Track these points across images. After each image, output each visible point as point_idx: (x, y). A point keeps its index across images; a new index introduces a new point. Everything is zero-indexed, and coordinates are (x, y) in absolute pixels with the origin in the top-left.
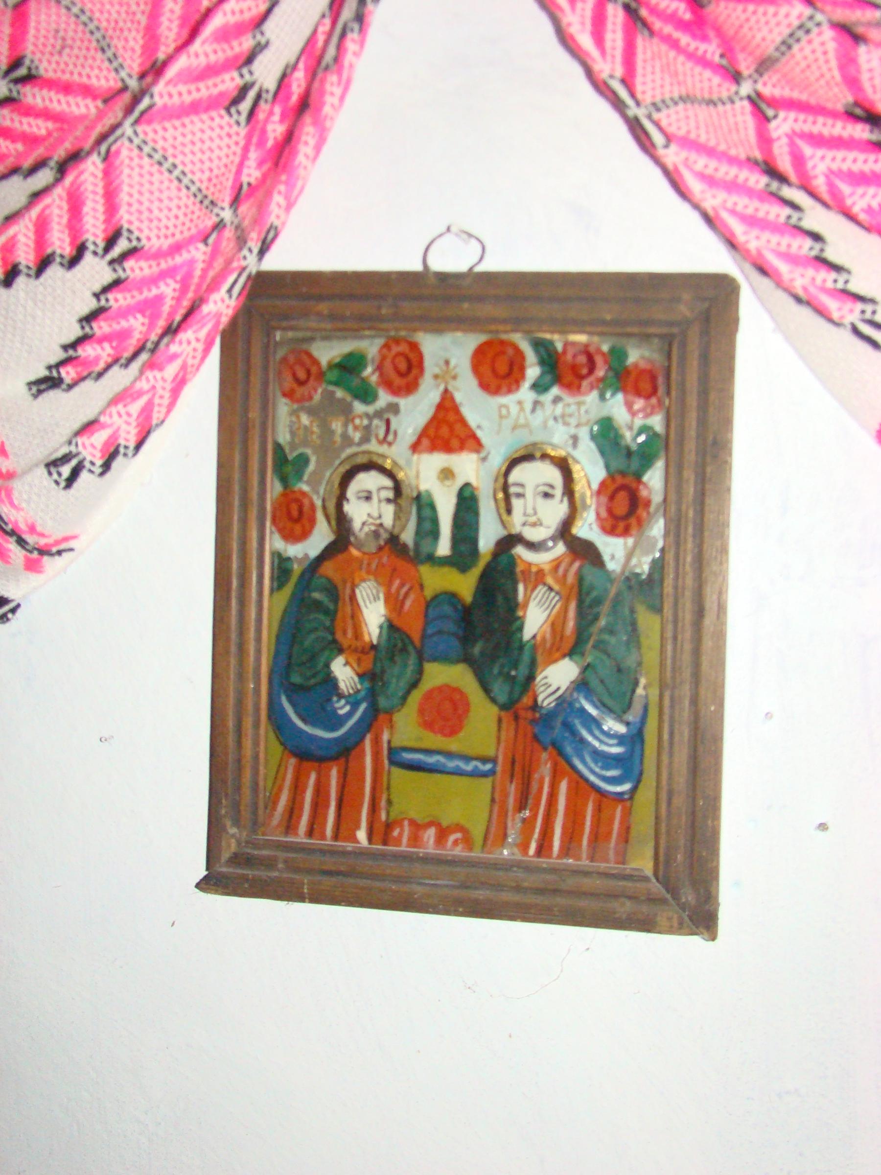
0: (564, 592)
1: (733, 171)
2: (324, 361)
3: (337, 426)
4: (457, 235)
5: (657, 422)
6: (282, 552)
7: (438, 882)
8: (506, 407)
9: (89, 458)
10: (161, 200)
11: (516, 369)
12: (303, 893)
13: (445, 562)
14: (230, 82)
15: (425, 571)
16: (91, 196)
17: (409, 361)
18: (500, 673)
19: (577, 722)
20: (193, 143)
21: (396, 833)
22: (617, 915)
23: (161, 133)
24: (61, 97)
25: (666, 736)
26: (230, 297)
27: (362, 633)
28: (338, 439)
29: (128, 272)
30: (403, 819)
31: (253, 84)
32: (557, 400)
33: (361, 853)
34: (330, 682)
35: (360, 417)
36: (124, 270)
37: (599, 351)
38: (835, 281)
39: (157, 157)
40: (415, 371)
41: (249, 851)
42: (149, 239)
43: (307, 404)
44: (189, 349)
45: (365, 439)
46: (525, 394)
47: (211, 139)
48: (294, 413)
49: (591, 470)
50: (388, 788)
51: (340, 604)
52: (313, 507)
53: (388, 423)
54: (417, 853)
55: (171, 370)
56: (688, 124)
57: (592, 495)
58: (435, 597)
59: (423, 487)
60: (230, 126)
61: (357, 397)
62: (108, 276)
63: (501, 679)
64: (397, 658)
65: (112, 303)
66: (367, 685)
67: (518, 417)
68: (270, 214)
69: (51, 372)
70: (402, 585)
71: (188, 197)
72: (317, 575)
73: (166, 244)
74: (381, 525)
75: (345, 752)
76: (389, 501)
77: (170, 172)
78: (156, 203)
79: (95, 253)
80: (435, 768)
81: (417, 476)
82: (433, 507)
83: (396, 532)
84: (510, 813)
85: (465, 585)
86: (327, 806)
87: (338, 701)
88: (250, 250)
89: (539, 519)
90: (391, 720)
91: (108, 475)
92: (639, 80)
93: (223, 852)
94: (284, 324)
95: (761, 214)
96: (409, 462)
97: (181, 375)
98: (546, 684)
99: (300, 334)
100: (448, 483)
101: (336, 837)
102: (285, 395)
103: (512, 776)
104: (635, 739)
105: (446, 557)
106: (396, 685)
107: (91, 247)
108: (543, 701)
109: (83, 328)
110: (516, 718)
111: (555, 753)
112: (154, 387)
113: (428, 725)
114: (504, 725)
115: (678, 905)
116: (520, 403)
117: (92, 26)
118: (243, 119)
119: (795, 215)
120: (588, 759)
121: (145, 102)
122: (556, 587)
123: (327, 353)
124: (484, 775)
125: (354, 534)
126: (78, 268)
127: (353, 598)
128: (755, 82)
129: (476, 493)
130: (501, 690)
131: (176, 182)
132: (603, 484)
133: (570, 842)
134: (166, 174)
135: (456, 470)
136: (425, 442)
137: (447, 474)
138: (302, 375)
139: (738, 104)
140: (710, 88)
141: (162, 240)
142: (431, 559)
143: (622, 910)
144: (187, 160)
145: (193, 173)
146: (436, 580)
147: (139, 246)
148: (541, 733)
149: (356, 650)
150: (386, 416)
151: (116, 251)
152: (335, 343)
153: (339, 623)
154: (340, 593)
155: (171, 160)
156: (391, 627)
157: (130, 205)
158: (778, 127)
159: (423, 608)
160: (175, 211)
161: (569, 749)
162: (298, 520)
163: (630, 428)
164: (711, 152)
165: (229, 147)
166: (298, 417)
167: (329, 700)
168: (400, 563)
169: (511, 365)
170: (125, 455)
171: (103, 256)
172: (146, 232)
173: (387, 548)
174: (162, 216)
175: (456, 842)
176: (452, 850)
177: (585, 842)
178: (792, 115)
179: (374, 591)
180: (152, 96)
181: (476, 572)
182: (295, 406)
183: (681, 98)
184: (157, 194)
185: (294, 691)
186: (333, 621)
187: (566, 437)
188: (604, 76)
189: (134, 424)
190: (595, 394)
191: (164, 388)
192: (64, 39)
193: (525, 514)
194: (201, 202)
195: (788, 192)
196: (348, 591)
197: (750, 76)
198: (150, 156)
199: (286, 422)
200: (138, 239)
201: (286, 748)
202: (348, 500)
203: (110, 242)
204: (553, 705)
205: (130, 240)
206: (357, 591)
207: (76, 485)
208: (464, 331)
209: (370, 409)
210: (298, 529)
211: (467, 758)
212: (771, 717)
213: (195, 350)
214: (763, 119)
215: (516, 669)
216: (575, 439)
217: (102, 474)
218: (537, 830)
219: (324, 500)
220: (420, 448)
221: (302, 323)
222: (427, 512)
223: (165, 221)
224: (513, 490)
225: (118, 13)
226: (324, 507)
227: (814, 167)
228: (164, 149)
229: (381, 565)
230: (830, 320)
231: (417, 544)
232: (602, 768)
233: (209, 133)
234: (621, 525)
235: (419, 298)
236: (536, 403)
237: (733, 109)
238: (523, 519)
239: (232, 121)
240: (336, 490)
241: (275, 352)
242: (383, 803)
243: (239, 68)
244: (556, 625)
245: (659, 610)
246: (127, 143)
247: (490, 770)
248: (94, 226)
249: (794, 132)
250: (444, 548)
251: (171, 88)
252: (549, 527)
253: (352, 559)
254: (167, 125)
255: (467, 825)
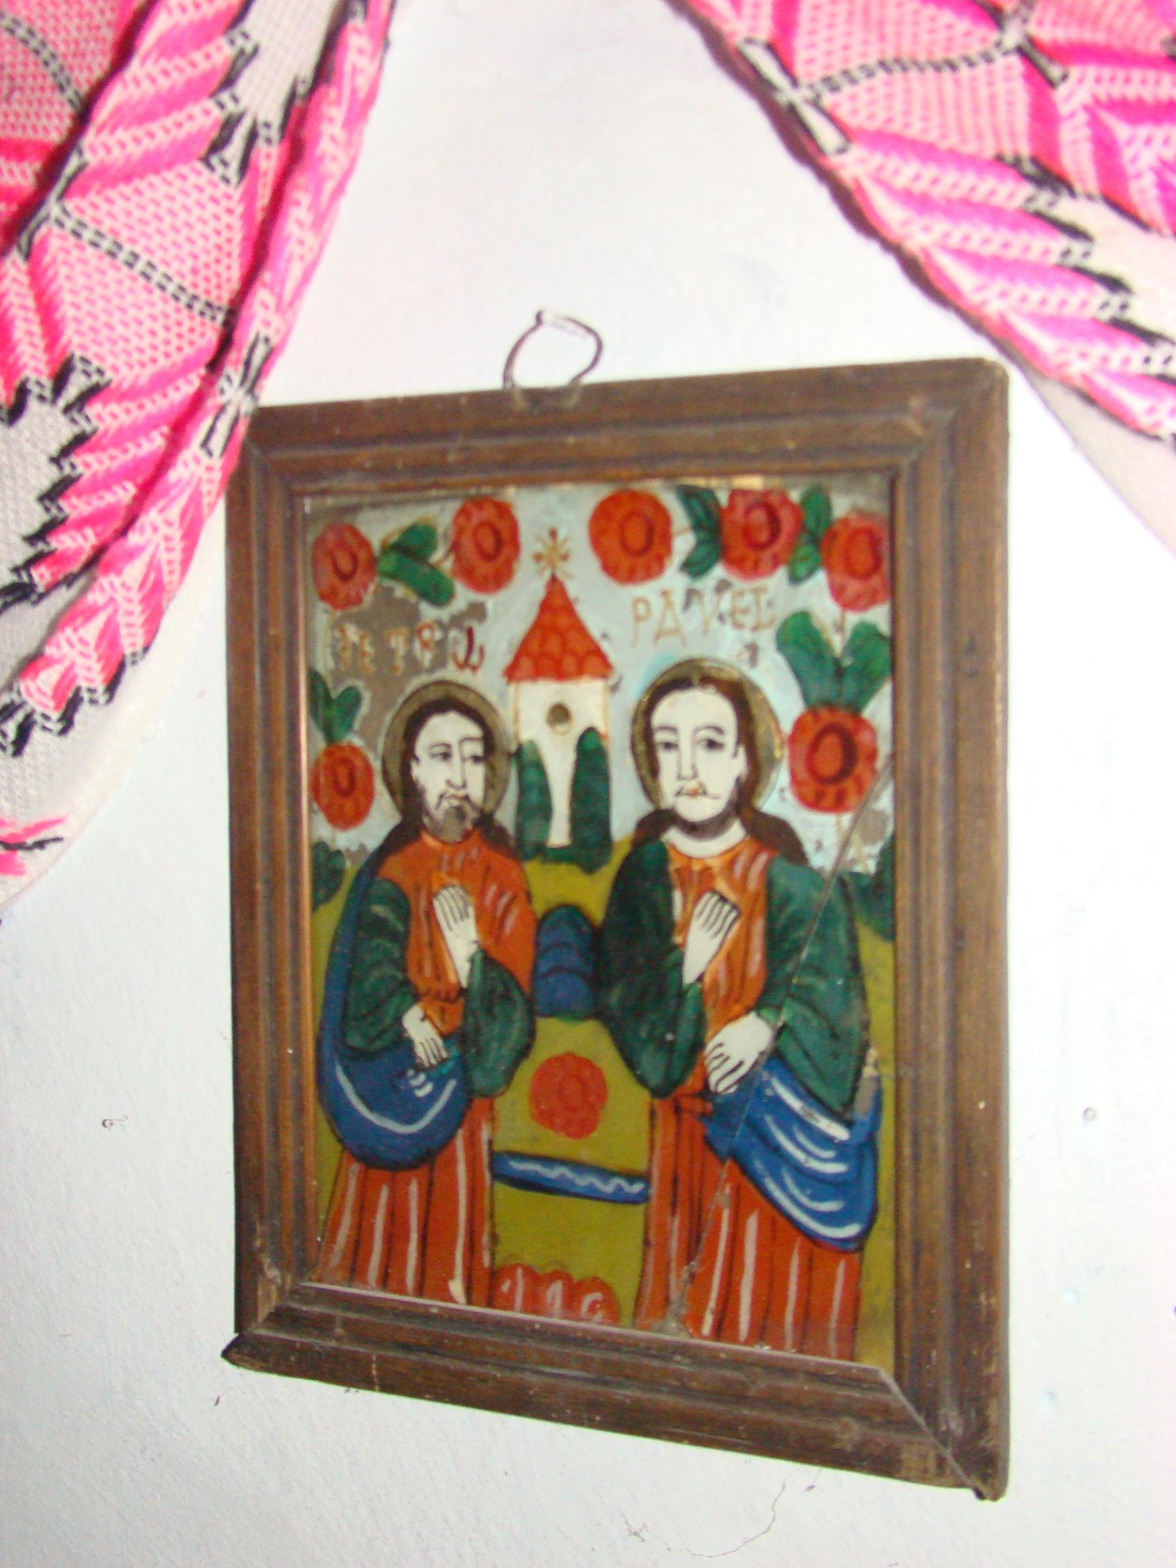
0: (743, 906)
1: (968, 180)
2: (376, 543)
3: (398, 642)
4: (555, 325)
5: (879, 616)
6: (329, 842)
7: (563, 1371)
8: (646, 602)
9: (39, 709)
10: (123, 310)
11: (657, 540)
12: (369, 1375)
13: (560, 856)
14: (203, 116)
15: (533, 870)
16: (21, 314)
17: (496, 533)
18: (651, 1036)
19: (769, 1119)
20: (158, 218)
21: (505, 1287)
22: (837, 1446)
23: (104, 207)
24: (14, 165)
25: (907, 1151)
26: (210, 454)
27: (445, 969)
28: (400, 663)
29: (95, 422)
30: (515, 1267)
31: (239, 118)
32: (722, 586)
33: (454, 1318)
34: (403, 1044)
35: (430, 627)
36: (88, 419)
37: (785, 500)
38: (1147, 360)
39: (106, 244)
40: (506, 551)
41: (295, 1305)
42: (115, 369)
43: (354, 610)
44: (158, 538)
45: (439, 662)
46: (673, 579)
47: (187, 209)
48: (337, 626)
49: (784, 699)
50: (492, 1216)
51: (413, 923)
52: (368, 769)
53: (470, 633)
54: (532, 1323)
55: (134, 572)
56: (889, 108)
57: (782, 744)
58: (548, 914)
59: (525, 736)
60: (215, 186)
61: (424, 595)
62: (66, 432)
63: (651, 1048)
64: (497, 1010)
65: (80, 469)
66: (455, 1052)
67: (663, 618)
68: (251, 318)
69: (19, 575)
70: (500, 894)
71: (165, 301)
72: (378, 879)
73: (145, 375)
74: (466, 798)
75: (428, 1155)
76: (476, 759)
77: (130, 265)
78: (117, 316)
79: (41, 398)
80: (559, 1186)
81: (516, 720)
82: (539, 767)
83: (489, 806)
84: (673, 1264)
85: (592, 893)
86: (407, 1240)
87: (416, 1076)
88: (229, 379)
89: (701, 785)
90: (491, 1108)
91: (72, 733)
92: (800, 42)
93: (260, 1306)
94: (311, 487)
95: (1013, 253)
96: (503, 696)
97: (152, 577)
98: (721, 1055)
99: (344, 501)
100: (561, 728)
101: (420, 1291)
102: (323, 597)
103: (674, 1205)
104: (862, 1151)
105: (563, 848)
106: (498, 1053)
107: (36, 390)
108: (717, 1084)
109: (47, 510)
110: (678, 1110)
111: (736, 1171)
112: (112, 600)
113: (545, 1117)
114: (659, 1123)
115: (936, 1434)
116: (665, 594)
117: (45, 54)
118: (233, 172)
119: (1077, 247)
120: (789, 1181)
121: (73, 163)
122: (732, 896)
123: (380, 527)
124: (633, 1201)
125: (428, 813)
126: (23, 422)
127: (430, 913)
128: (1025, 21)
129: (604, 743)
130: (652, 1063)
131: (142, 281)
132: (799, 725)
133: (765, 1318)
134: (125, 269)
135: (573, 708)
136: (526, 663)
137: (560, 714)
138: (345, 564)
139: (1000, 62)
140: (950, 40)
141: (137, 369)
142: (541, 851)
143: (846, 1437)
144: (153, 245)
145: (166, 263)
146: (552, 885)
147: (103, 381)
148: (718, 1136)
149: (437, 996)
150: (467, 623)
151: (72, 391)
152: (390, 512)
153: (412, 957)
154: (412, 903)
155: (128, 247)
156: (486, 960)
157: (77, 320)
158: (1068, 98)
159: (532, 930)
160: (148, 324)
161: (758, 1165)
162: (347, 793)
163: (840, 628)
164: (927, 152)
165: (217, 218)
166: (343, 631)
167: (402, 1074)
168: (498, 860)
169: (650, 531)
170: (93, 702)
171: (54, 401)
172: (110, 360)
173: (475, 837)
174: (129, 333)
175: (592, 1309)
176: (588, 1320)
177: (789, 1317)
178: (1091, 71)
179: (461, 904)
180: (81, 153)
181: (609, 872)
182: (339, 613)
183: (882, 64)
184: (116, 301)
185: (356, 1059)
186: (404, 948)
187: (738, 647)
188: (738, 40)
189: (94, 656)
190: (782, 573)
191: (130, 601)
192: (12, 78)
193: (680, 777)
194: (190, 307)
195: (1066, 209)
196: (423, 903)
197: (1016, 12)
198: (95, 245)
199: (325, 639)
200: (100, 372)
201: (344, 1147)
202: (417, 759)
203: (60, 379)
204: (732, 1090)
205: (87, 374)
206: (436, 904)
207: (28, 749)
208: (575, 480)
209: (444, 614)
210: (349, 805)
211: (606, 1173)
212: (1094, 1117)
213: (167, 539)
214: (1040, 84)
215: (674, 1032)
216: (753, 650)
217: (64, 732)
218: (714, 1295)
219: (384, 762)
220: (518, 674)
221: (334, 483)
222: (532, 776)
223: (135, 341)
224: (660, 737)
225: (79, 29)
226: (385, 773)
227: (1134, 159)
228: (114, 232)
229: (468, 862)
230: (1139, 431)
231: (519, 828)
232: (814, 1197)
233: (181, 199)
234: (831, 791)
235: (503, 432)
236: (691, 595)
237: (990, 73)
238: (677, 785)
239: (216, 177)
240: (400, 746)
241: (305, 533)
242: (485, 1239)
243: (212, 95)
244: (734, 960)
245: (891, 935)
246: (56, 229)
247: (640, 1194)
248: (33, 357)
249: (1097, 101)
250: (559, 834)
251: (105, 136)
252: (716, 797)
253: (429, 852)
254: (111, 193)
255: (610, 1280)
